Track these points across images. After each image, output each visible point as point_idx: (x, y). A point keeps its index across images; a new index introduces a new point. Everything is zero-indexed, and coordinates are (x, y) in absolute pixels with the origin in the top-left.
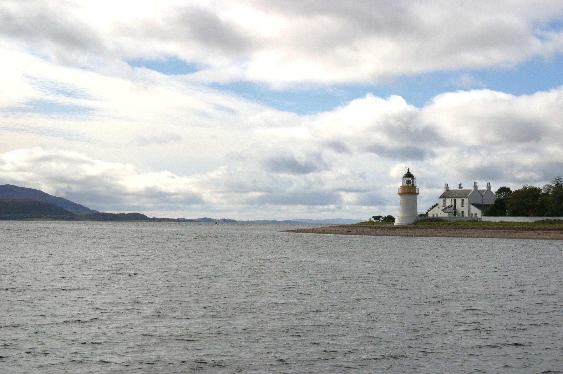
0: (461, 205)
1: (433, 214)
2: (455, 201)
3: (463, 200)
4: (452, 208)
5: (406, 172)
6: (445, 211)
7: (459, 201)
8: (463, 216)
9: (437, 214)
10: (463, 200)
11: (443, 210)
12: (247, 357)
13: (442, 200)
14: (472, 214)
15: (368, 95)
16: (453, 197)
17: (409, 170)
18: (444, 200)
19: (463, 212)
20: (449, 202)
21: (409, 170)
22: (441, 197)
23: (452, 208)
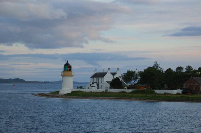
5: (66, 63)
17: (67, 61)
20: (95, 79)
21: (67, 61)
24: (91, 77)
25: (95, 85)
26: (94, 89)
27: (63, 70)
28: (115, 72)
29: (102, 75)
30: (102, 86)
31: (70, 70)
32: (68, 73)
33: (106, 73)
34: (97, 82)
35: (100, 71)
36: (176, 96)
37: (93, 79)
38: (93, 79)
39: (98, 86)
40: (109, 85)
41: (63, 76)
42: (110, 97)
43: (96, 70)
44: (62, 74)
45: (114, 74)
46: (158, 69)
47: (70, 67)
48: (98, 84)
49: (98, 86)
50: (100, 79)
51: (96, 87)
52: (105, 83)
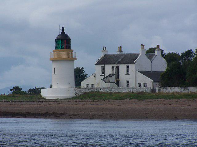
0: (125, 73)
1: (88, 85)
2: (118, 67)
3: (128, 67)
4: (114, 77)
5: (59, 32)
6: (106, 80)
7: (123, 68)
8: (128, 86)
9: (93, 85)
10: (128, 67)
11: (103, 80)
12: (50, 128)
13: (99, 67)
14: (140, 84)
15: (180, 54)
16: (114, 63)
17: (63, 29)
18: (102, 68)
19: (128, 82)
20: (109, 69)
21: (63, 29)
22: (98, 63)
23: (114, 77)
31: (69, 48)
44: (53, 57)
50: (123, 68)
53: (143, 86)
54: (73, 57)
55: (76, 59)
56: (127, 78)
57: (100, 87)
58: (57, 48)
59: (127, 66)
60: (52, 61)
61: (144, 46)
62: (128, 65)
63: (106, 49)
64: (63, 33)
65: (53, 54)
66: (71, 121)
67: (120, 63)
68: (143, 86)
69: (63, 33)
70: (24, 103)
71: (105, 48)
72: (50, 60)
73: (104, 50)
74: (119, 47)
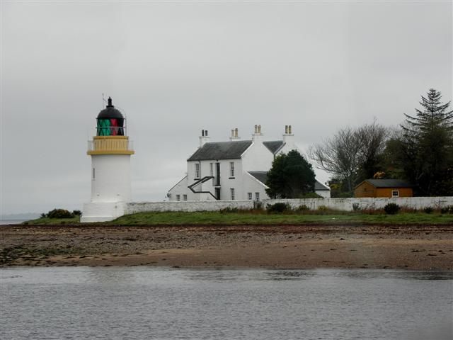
5: (104, 106)
13: (193, 164)
17: (110, 100)
20: (207, 168)
21: (110, 100)
24: (188, 161)
25: (209, 186)
26: (204, 202)
27: (95, 134)
28: (249, 139)
29: (235, 151)
30: (232, 189)
31: (120, 133)
32: (113, 143)
33: (246, 145)
34: (215, 175)
35: (220, 136)
36: (425, 216)
37: (198, 167)
38: (198, 167)
39: (218, 191)
40: (262, 187)
41: (94, 155)
42: (424, 227)
43: (205, 133)
44: (93, 149)
45: (273, 147)
46: (446, 147)
47: (119, 121)
48: (218, 184)
49: (218, 191)
50: (225, 165)
51: (214, 192)
52: (244, 185)
53: (182, 197)
54: (130, 149)
55: (133, 153)
56: (232, 184)
57: (316, 188)
58: (100, 132)
59: (197, 165)
60: (92, 155)
61: (260, 127)
62: (232, 161)
63: (207, 135)
64: (110, 105)
65: (93, 145)
66: (129, 268)
67: (224, 158)
68: (182, 197)
69: (110, 105)
70: (55, 237)
71: (205, 133)
72: (88, 154)
73: (203, 135)
74: (233, 131)
